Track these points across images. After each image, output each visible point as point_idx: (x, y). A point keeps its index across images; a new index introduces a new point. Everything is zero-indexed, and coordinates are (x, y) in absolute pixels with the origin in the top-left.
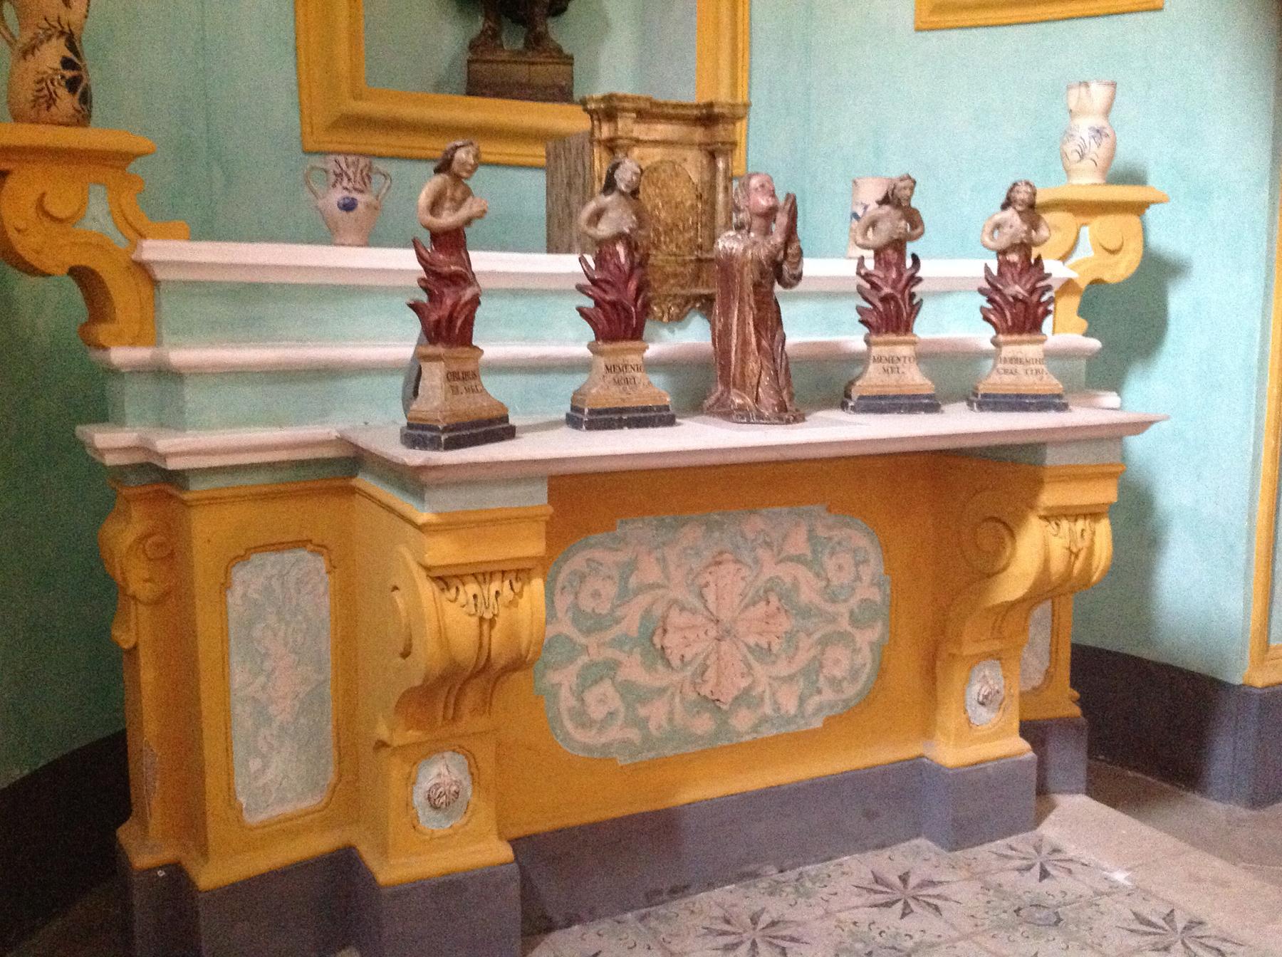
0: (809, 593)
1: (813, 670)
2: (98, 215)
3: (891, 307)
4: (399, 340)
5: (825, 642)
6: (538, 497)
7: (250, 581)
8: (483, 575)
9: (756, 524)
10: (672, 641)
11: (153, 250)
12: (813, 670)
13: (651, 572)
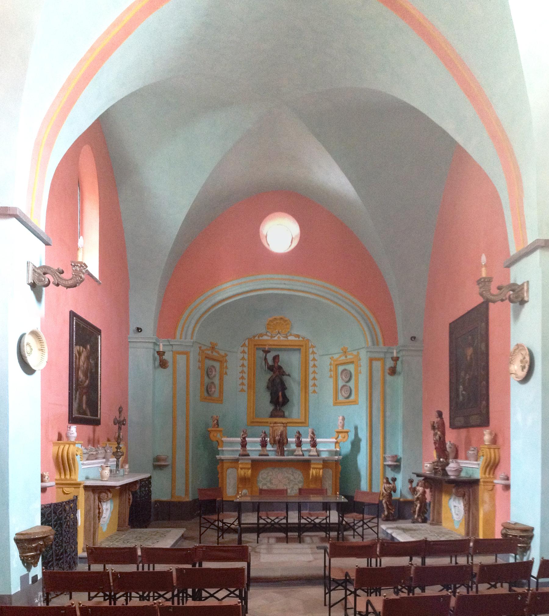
0: (292, 478)
1: (293, 488)
2: (219, 436)
3: (299, 444)
4: (239, 448)
5: (294, 484)
6: (250, 462)
7: (229, 471)
8: (245, 468)
9: (284, 469)
10: (273, 482)
11: (223, 439)
12: (293, 488)
13: (271, 473)
